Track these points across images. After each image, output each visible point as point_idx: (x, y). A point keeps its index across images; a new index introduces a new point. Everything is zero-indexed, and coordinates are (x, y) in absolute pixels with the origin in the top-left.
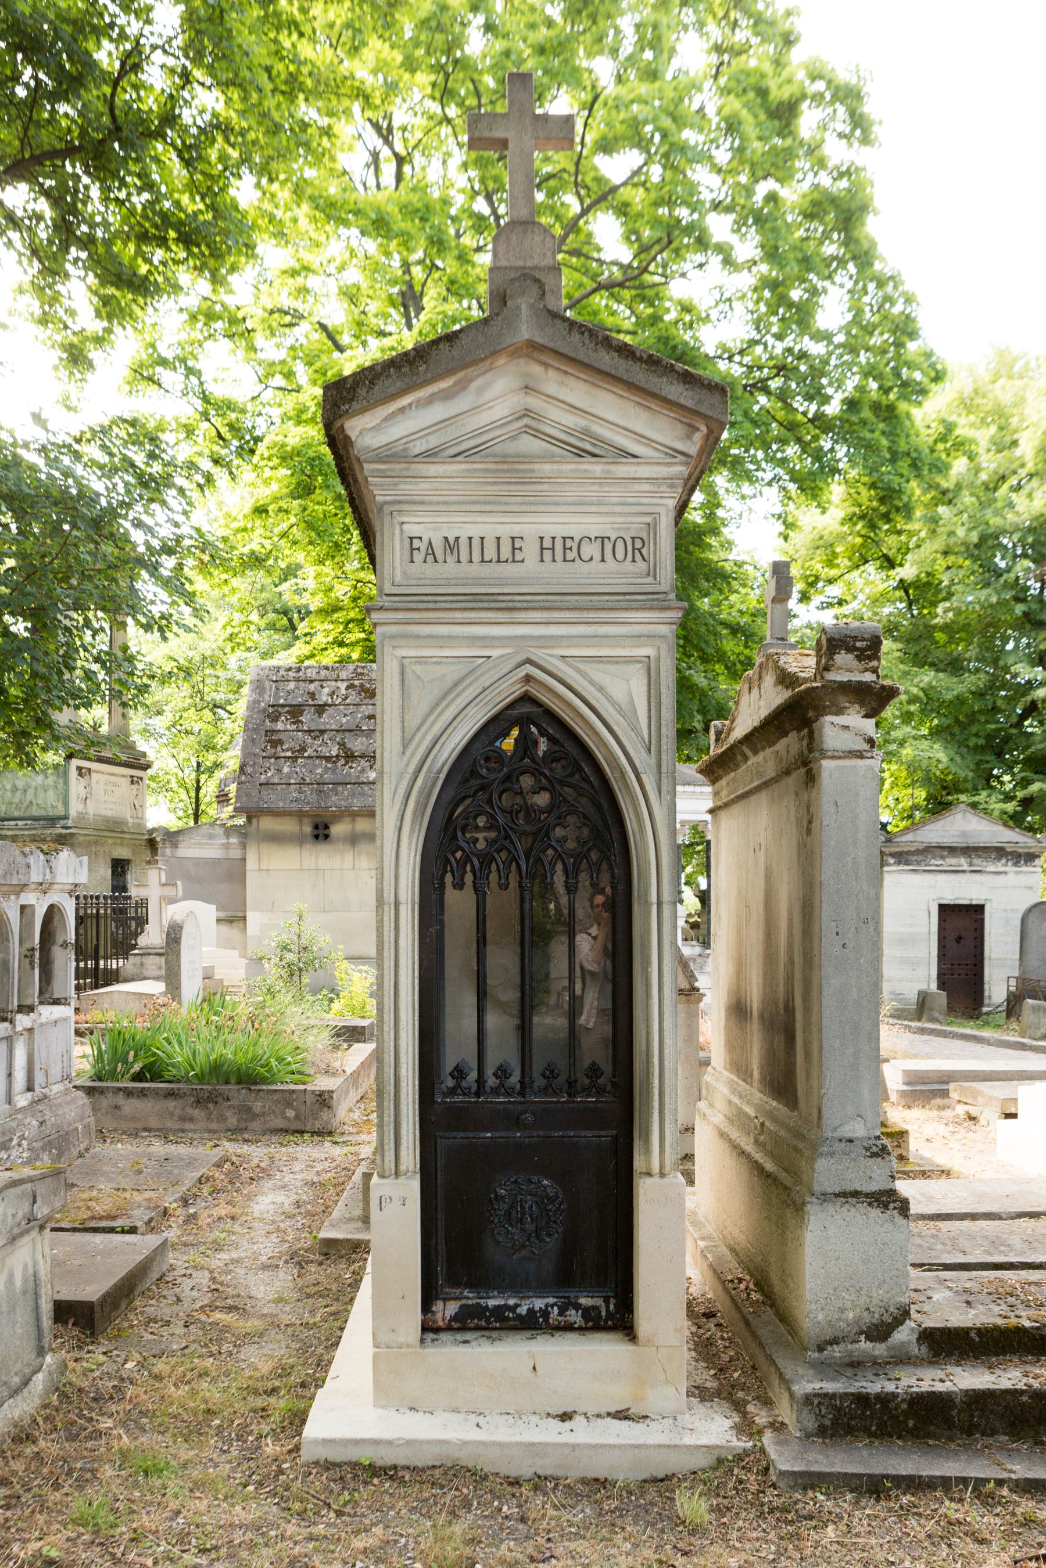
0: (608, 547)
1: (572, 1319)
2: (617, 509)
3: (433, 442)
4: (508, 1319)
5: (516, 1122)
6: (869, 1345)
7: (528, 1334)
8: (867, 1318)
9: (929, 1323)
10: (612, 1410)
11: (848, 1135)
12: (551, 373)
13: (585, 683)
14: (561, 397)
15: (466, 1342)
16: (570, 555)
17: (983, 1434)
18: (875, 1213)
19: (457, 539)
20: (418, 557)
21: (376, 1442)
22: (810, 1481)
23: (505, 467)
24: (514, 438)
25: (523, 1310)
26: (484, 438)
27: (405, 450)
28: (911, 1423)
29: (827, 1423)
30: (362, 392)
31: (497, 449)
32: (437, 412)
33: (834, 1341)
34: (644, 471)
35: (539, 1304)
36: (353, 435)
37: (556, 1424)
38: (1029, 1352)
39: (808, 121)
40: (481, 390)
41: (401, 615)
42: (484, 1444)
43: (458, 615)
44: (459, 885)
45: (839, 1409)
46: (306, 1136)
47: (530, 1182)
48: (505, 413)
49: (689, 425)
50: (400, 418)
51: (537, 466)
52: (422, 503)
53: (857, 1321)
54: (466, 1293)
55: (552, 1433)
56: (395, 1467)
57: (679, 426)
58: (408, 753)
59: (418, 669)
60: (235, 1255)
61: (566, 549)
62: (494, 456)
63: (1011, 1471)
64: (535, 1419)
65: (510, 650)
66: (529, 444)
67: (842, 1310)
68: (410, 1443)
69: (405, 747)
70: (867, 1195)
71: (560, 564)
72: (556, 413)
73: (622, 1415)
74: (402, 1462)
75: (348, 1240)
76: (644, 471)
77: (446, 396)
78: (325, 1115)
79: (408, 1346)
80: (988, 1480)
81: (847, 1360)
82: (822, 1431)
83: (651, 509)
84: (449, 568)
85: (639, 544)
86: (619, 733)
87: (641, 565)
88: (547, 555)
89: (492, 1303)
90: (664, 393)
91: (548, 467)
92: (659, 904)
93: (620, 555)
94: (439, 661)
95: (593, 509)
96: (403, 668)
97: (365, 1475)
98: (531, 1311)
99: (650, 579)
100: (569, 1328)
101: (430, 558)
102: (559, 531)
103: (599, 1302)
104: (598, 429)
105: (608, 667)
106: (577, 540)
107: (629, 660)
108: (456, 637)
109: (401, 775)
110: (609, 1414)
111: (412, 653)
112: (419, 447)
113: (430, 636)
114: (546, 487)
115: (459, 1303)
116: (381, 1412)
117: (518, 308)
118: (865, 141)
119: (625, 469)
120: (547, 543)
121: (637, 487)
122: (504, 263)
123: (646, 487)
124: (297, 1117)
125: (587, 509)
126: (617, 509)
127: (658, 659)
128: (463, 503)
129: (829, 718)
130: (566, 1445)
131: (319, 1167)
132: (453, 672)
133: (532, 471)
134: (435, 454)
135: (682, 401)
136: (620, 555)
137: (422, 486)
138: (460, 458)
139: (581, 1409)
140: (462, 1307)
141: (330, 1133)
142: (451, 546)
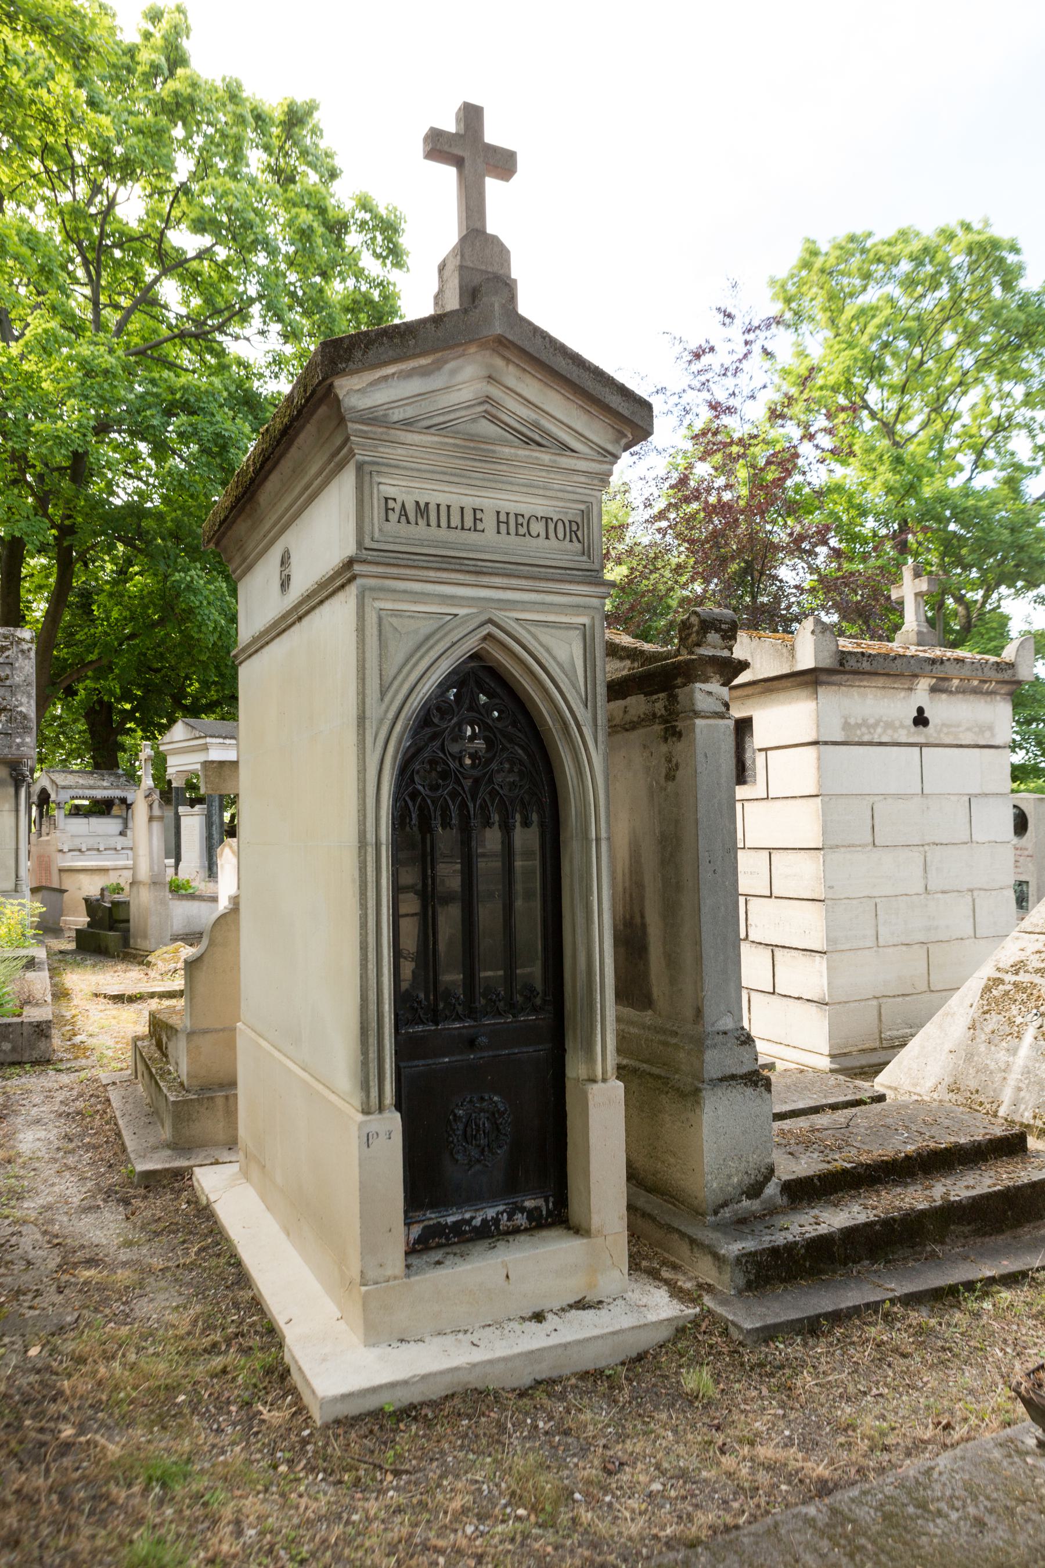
0: (551, 526)
1: (518, 1222)
2: (560, 495)
3: (410, 412)
4: (465, 1232)
5: (471, 1043)
6: (749, 1202)
7: (486, 1243)
8: (747, 1180)
9: (786, 1177)
10: (571, 1301)
11: (722, 1028)
12: (511, 368)
13: (536, 644)
14: (519, 390)
15: (439, 1263)
16: (522, 530)
17: (854, 1262)
18: (749, 1091)
19: (427, 504)
20: (393, 517)
21: (393, 1385)
22: (768, 1334)
23: (472, 445)
24: (474, 420)
25: (477, 1222)
26: (452, 416)
27: (385, 415)
28: (808, 1264)
29: (752, 1277)
30: (358, 354)
31: (460, 427)
32: (415, 386)
33: (725, 1205)
34: (582, 465)
35: (491, 1213)
36: (341, 394)
37: (533, 1326)
38: (851, 1188)
39: (353, 239)
40: (453, 372)
41: (380, 569)
42: (490, 1362)
43: (432, 574)
44: (526, 823)
45: (759, 1264)
46: (27, 1067)
47: (482, 1099)
48: (471, 396)
49: (619, 431)
50: (383, 385)
51: (498, 448)
52: (397, 467)
53: (740, 1182)
54: (428, 1215)
55: (534, 1339)
56: (413, 1406)
57: (611, 430)
58: (387, 699)
59: (394, 621)
60: (41, 1201)
61: (513, 524)
62: (458, 433)
63: (892, 1290)
64: (515, 1325)
65: (474, 610)
66: (486, 428)
67: (729, 1177)
68: (424, 1378)
69: (383, 694)
70: (741, 1077)
71: (513, 537)
72: (511, 403)
73: (581, 1305)
74: (416, 1400)
75: (167, 1170)
76: (582, 465)
77: (424, 372)
78: (42, 1045)
79: (395, 1278)
80: (884, 1301)
81: (735, 1218)
82: (750, 1286)
83: (585, 499)
84: (420, 530)
85: (574, 528)
86: (564, 690)
87: (577, 546)
88: (503, 527)
89: (450, 1220)
90: (607, 401)
91: (507, 450)
92: (598, 840)
93: (561, 535)
94: (413, 616)
95: (541, 492)
96: (380, 618)
97: (384, 1424)
98: (484, 1221)
99: (585, 558)
100: (516, 1231)
101: (403, 518)
102: (513, 508)
103: (540, 1202)
104: (546, 423)
105: (553, 631)
106: (527, 517)
107: (569, 627)
108: (428, 594)
109: (381, 721)
110: (571, 1306)
111: (389, 605)
112: (397, 415)
113: (405, 592)
114: (504, 468)
115: (421, 1226)
116: (376, 1351)
117: (492, 305)
118: (398, 264)
119: (566, 462)
120: (503, 518)
121: (576, 478)
122: (470, 264)
123: (583, 479)
124: (14, 1049)
125: (537, 491)
126: (560, 495)
127: (593, 626)
128: (433, 472)
129: (698, 685)
130: (560, 1345)
131: (60, 1096)
132: (426, 627)
133: (494, 452)
134: (410, 424)
135: (621, 410)
136: (561, 535)
137: (399, 451)
138: (432, 430)
139: (547, 1307)
140: (424, 1228)
141: (48, 1062)
142: (422, 510)
